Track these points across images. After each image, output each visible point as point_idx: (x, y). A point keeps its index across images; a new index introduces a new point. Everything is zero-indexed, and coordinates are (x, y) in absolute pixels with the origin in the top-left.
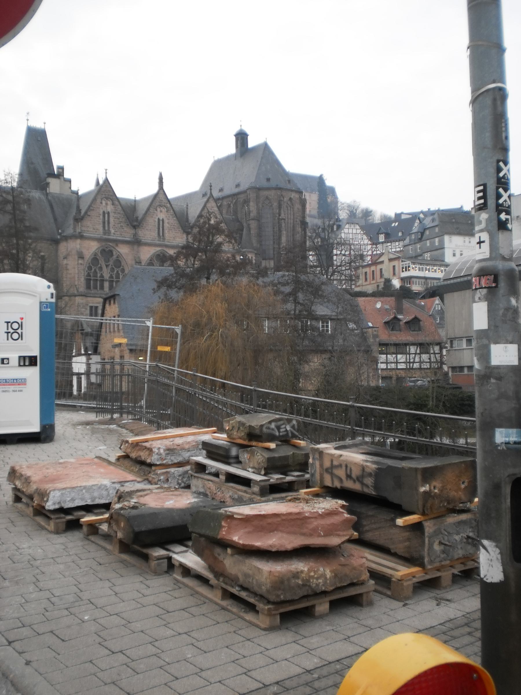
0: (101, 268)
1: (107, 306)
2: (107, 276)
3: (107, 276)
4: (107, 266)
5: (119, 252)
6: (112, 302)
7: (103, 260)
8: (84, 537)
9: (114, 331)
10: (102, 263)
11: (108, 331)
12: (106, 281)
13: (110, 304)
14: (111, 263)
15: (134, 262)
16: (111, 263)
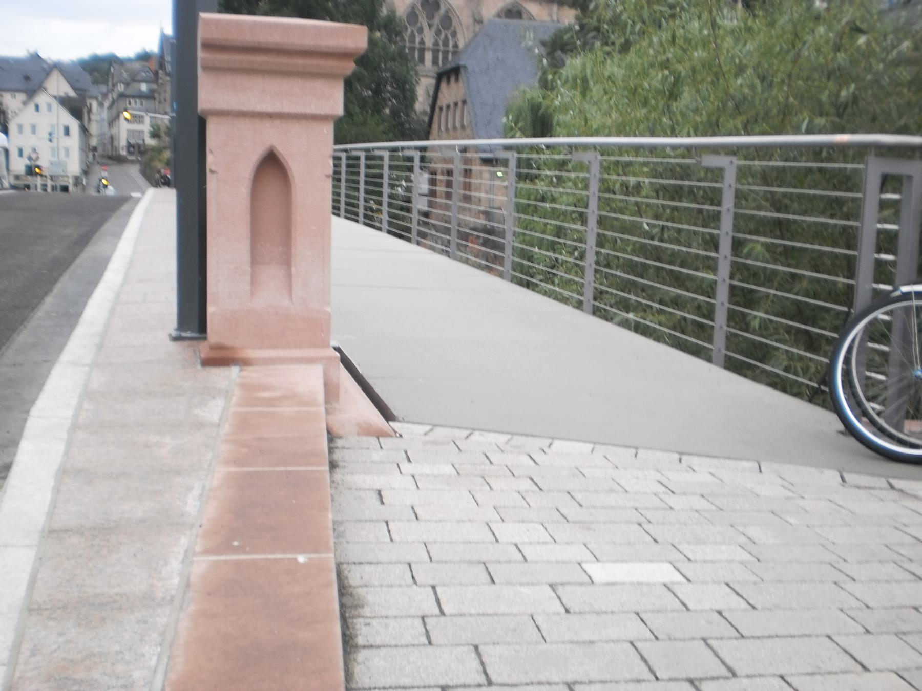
0: (421, 30)
1: (443, 86)
2: (429, 41)
3: (429, 41)
4: (430, 26)
5: (449, 4)
6: (453, 79)
7: (425, 17)
8: (85, 90)
9: (455, 128)
10: (423, 21)
11: (443, 128)
12: (429, 49)
13: (448, 82)
14: (436, 21)
15: (471, 21)
16: (436, 21)
